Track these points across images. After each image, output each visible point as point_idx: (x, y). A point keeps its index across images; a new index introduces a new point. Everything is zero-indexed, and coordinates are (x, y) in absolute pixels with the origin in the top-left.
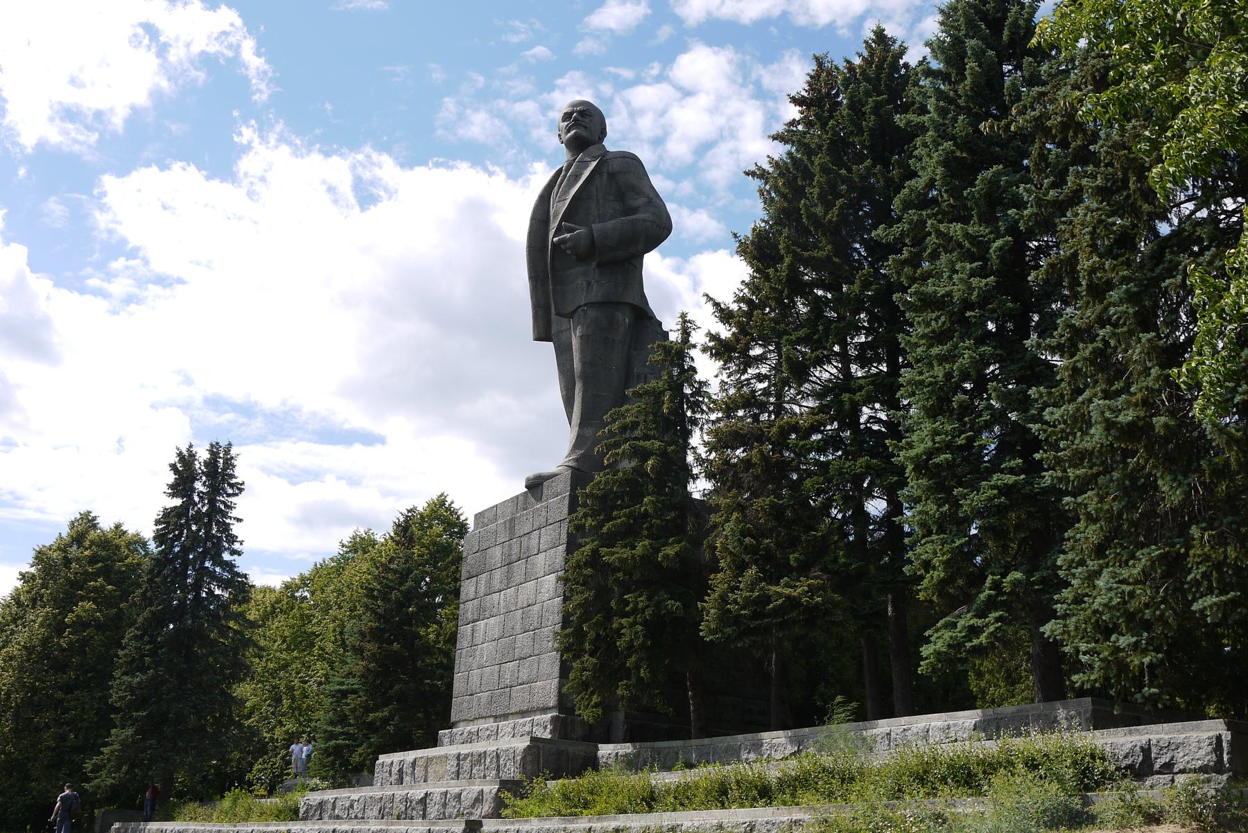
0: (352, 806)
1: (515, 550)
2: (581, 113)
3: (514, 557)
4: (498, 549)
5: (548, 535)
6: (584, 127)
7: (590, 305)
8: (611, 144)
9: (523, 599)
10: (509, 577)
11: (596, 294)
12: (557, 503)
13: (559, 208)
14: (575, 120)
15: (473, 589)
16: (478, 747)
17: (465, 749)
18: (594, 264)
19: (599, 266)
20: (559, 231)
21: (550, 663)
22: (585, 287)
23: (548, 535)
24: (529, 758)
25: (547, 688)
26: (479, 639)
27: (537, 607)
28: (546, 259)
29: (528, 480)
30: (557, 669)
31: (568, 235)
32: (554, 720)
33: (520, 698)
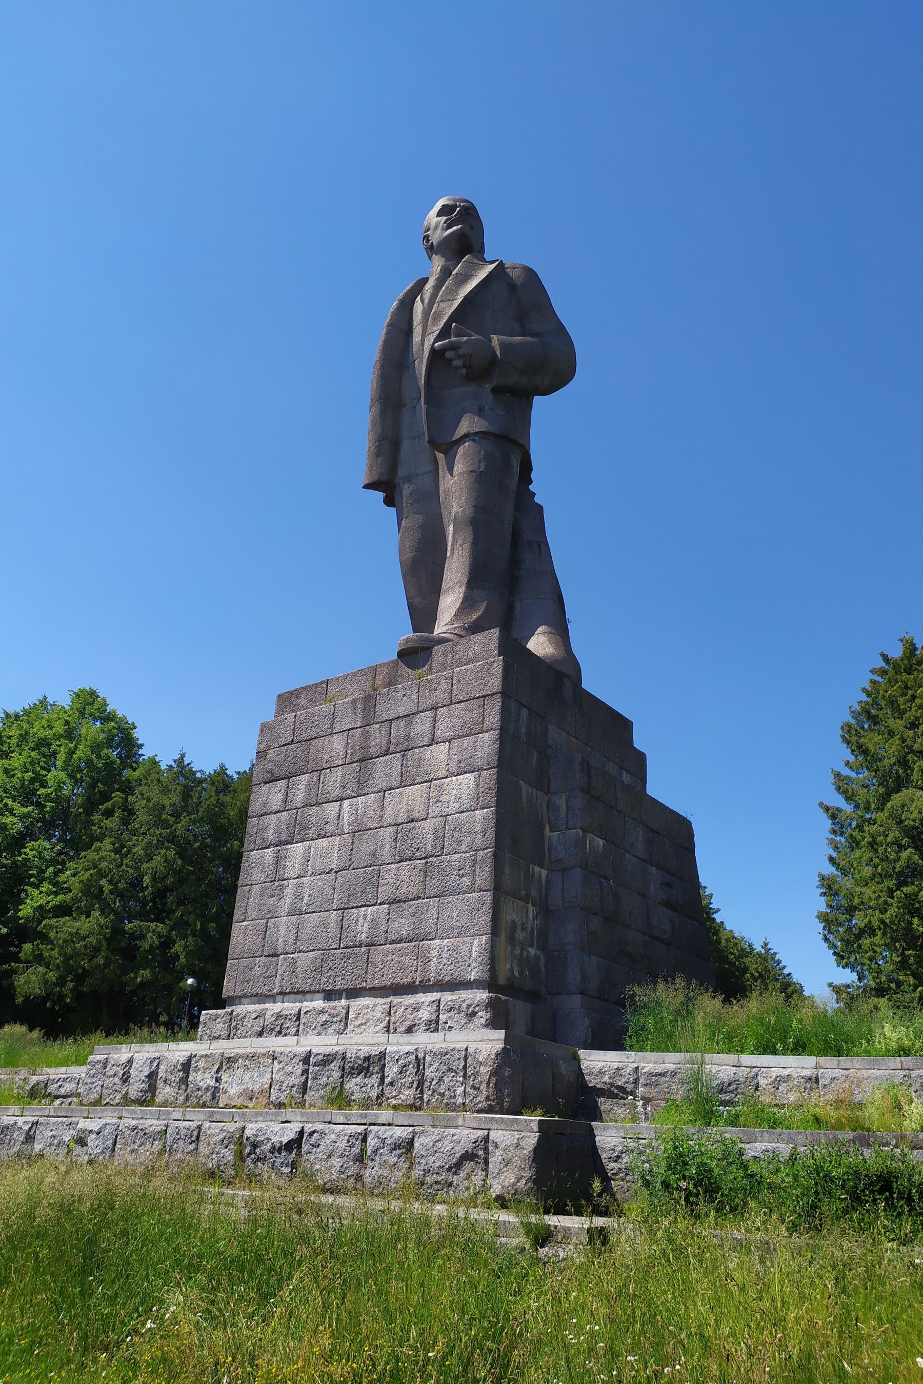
15: (280, 796)
18: (488, 387)
27: (429, 825)
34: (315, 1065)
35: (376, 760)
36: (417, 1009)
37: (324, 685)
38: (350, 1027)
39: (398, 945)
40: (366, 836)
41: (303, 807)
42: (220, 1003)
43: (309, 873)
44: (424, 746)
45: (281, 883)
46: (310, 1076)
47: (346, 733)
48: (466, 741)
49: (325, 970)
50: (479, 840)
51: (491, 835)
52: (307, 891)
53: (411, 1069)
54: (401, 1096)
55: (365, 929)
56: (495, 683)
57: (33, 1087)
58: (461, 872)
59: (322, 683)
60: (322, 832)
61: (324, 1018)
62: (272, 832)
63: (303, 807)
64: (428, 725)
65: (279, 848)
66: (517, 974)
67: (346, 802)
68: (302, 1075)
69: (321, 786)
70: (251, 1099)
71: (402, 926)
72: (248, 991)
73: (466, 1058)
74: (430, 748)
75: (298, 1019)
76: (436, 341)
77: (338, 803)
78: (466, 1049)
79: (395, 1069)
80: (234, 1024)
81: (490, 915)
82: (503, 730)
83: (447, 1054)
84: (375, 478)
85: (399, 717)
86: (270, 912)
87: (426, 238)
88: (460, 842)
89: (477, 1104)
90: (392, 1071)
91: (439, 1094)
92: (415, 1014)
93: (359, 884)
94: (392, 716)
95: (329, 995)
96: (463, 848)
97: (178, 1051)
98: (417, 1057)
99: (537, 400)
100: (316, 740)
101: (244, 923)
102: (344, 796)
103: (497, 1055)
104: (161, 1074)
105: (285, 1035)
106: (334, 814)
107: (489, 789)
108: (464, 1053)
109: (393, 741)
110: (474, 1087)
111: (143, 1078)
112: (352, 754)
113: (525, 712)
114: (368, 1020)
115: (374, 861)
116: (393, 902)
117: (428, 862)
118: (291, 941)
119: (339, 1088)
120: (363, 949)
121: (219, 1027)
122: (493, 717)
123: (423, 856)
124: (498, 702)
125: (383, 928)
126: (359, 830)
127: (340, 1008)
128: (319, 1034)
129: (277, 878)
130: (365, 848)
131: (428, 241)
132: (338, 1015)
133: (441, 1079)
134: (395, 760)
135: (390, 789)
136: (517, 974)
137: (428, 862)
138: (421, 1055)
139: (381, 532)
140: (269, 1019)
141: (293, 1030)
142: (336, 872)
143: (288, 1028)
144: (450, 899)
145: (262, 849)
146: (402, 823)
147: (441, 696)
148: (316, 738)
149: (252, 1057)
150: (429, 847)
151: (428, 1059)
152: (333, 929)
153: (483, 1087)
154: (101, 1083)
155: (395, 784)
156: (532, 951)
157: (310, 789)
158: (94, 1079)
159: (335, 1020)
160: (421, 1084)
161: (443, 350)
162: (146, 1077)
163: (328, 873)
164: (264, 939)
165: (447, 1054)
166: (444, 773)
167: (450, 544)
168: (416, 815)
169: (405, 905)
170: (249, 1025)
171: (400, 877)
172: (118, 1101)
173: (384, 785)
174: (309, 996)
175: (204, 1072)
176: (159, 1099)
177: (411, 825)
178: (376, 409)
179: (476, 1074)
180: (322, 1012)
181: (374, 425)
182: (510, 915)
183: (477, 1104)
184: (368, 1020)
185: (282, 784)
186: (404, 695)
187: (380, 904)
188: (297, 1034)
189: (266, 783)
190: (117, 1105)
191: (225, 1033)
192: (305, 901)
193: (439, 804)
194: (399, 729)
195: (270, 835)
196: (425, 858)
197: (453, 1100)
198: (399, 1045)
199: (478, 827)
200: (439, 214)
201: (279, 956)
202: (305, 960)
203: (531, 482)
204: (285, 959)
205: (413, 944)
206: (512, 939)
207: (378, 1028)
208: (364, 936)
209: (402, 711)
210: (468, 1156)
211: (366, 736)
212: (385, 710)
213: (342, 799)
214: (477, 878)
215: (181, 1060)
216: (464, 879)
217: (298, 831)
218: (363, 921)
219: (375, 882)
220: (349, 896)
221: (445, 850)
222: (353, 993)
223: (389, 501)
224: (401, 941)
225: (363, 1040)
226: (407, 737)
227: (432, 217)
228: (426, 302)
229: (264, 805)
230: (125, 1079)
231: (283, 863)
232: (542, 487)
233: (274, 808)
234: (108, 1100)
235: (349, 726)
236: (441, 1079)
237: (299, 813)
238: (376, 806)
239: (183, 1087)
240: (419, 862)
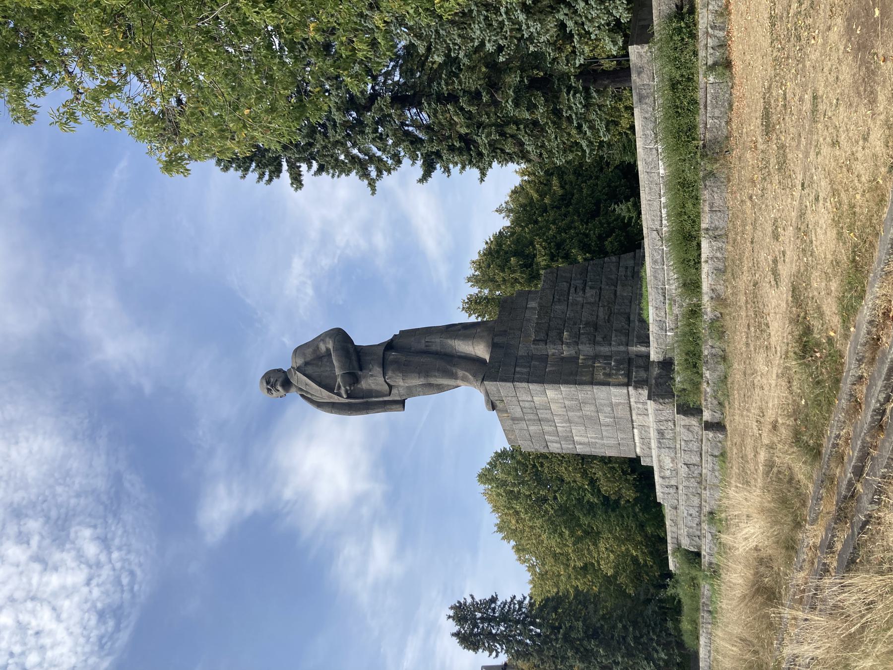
0: (691, 515)
1: (532, 417)
2: (268, 383)
3: (536, 418)
4: (531, 428)
5: (524, 396)
6: (278, 380)
7: (384, 375)
8: (366, 182)
9: (561, 411)
10: (547, 420)
11: (377, 370)
12: (503, 389)
13: (324, 395)
14: (272, 386)
15: (555, 445)
16: (653, 434)
17: (654, 444)
18: (360, 373)
19: (361, 370)
20: (339, 395)
21: (600, 392)
22: (373, 381)
23: (524, 396)
24: (661, 401)
25: (617, 394)
26: (586, 440)
27: (567, 403)
28: (355, 404)
29: (489, 410)
30: (604, 388)
31: (343, 388)
32: (636, 388)
33: (621, 412)
56: (510, 384)
113: (518, 369)
116: (598, 412)
121: (648, 460)
149: (659, 461)
156: (613, 363)
171: (588, 410)
182: (600, 376)
206: (609, 375)
210: (688, 429)
212: (518, 412)
217: (570, 439)
219: (590, 418)
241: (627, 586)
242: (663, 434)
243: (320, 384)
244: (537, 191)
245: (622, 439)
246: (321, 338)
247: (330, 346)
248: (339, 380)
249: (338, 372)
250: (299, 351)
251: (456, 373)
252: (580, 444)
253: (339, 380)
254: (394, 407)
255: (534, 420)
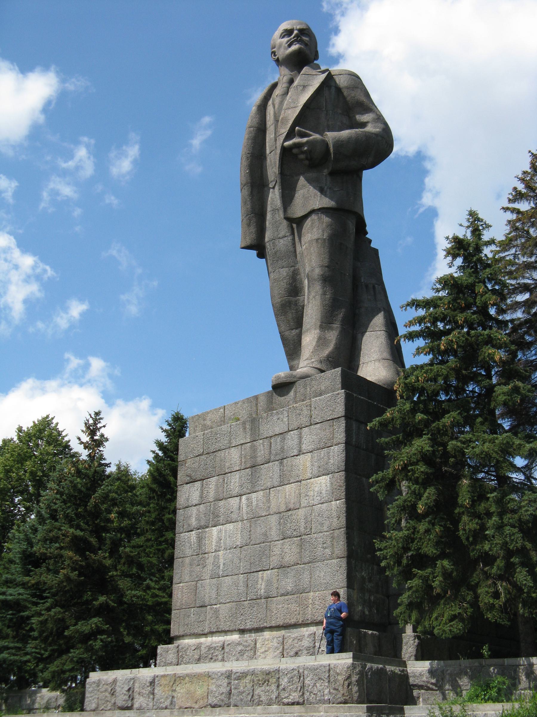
5: (310, 437)
18: (326, 172)
19: (332, 174)
24: (355, 678)
27: (301, 513)
33: (281, 610)
34: (235, 679)
35: (262, 466)
36: (300, 640)
37: (222, 410)
38: (258, 654)
39: (286, 597)
40: (259, 522)
41: (215, 501)
42: (170, 640)
43: (223, 548)
44: (295, 456)
45: (204, 555)
46: (233, 687)
47: (239, 447)
48: (323, 452)
49: (239, 615)
50: (335, 523)
51: (343, 521)
52: (222, 561)
53: (296, 679)
54: (291, 697)
55: (263, 587)
56: (340, 409)
57: (48, 701)
58: (325, 545)
59: (220, 409)
60: (229, 519)
61: (240, 648)
62: (194, 519)
63: (215, 501)
64: (296, 441)
65: (200, 530)
66: (367, 613)
67: (244, 497)
68: (228, 686)
69: (225, 485)
70: (196, 703)
71: (288, 584)
72: (188, 631)
73: (329, 671)
74: (298, 457)
75: (223, 648)
76: (286, 139)
77: (239, 498)
78: (329, 665)
79: (286, 680)
80: (180, 654)
81: (345, 575)
82: (348, 443)
83: (317, 669)
84: (248, 242)
85: (276, 435)
86: (197, 576)
87: (274, 53)
88: (322, 524)
89: (338, 699)
90: (284, 682)
91: (314, 694)
92: (300, 643)
93: (255, 556)
94: (271, 434)
95: (242, 631)
96: (325, 528)
97: (144, 674)
98: (298, 671)
99: (365, 173)
100: (219, 452)
101: (181, 585)
102: (242, 493)
103: (348, 668)
104: (136, 689)
105: (215, 660)
106: (236, 506)
107: (340, 486)
108: (328, 668)
109: (273, 452)
110: (335, 689)
111: (125, 692)
112: (245, 462)
114: (269, 648)
115: (266, 540)
117: (301, 537)
118: (214, 596)
119: (251, 694)
120: (263, 600)
122: (340, 435)
123: (299, 535)
124: (342, 423)
125: (275, 585)
126: (255, 518)
127: (250, 641)
128: (237, 660)
129: (201, 553)
130: (259, 530)
131: (275, 55)
132: (249, 646)
133: (315, 685)
134: (275, 466)
135: (273, 488)
136: (367, 613)
137: (301, 537)
138: (301, 671)
139: (257, 280)
140: (203, 650)
141: (220, 657)
142: (241, 547)
143: (217, 656)
144: (317, 564)
145: (188, 532)
146: (283, 512)
147: (304, 420)
148: (219, 450)
150: (302, 529)
151: (306, 672)
152: (242, 589)
153: (340, 688)
154: (97, 696)
155: (276, 484)
157: (218, 488)
158: (92, 694)
159: (247, 649)
160: (303, 687)
161: (291, 148)
162: (127, 691)
163: (235, 548)
164: (195, 595)
165: (317, 669)
166: (309, 475)
167: (306, 294)
168: (292, 506)
169: (288, 570)
170: (191, 655)
172: (109, 708)
173: (269, 484)
174: (229, 633)
175: (165, 687)
176: (136, 705)
177: (290, 513)
178: (246, 192)
179: (335, 681)
180: (239, 644)
181: (244, 203)
183: (338, 699)
184: (269, 648)
185: (198, 484)
186: (278, 419)
187: (272, 569)
188: (223, 660)
189: (187, 483)
190: (109, 710)
191: (175, 661)
192: (221, 568)
193: (307, 498)
194: (276, 443)
195: (194, 522)
196: (300, 536)
197: (322, 698)
198: (288, 664)
199: (335, 514)
200: (282, 36)
201: (206, 606)
202: (224, 610)
203: (367, 233)
204: (211, 609)
205: (295, 596)
207: (276, 654)
208: (262, 591)
209: (277, 430)
211: (254, 449)
213: (241, 495)
214: (335, 549)
215: (148, 679)
216: (327, 550)
218: (262, 581)
220: (251, 563)
221: (313, 530)
222: (259, 630)
223: (261, 255)
224: (287, 594)
225: (266, 662)
226: (282, 449)
227: (277, 37)
228: (276, 106)
229: (188, 500)
230: (113, 693)
231: (204, 542)
232: (376, 234)
233: (195, 502)
234: (103, 707)
235: (242, 442)
236: (315, 685)
237: (212, 506)
238: (264, 500)
239: (152, 696)
240: (296, 539)
241: (492, 453)
242: (266, 681)
243: (307, 106)
244: (17, 642)
245: (217, 611)
246: (380, 118)
247: (370, 128)
248: (316, 136)
249: (331, 136)
250: (356, 81)
251: (332, 329)
252: (200, 539)
253: (316, 136)
254: (253, 229)
255: (254, 457)
